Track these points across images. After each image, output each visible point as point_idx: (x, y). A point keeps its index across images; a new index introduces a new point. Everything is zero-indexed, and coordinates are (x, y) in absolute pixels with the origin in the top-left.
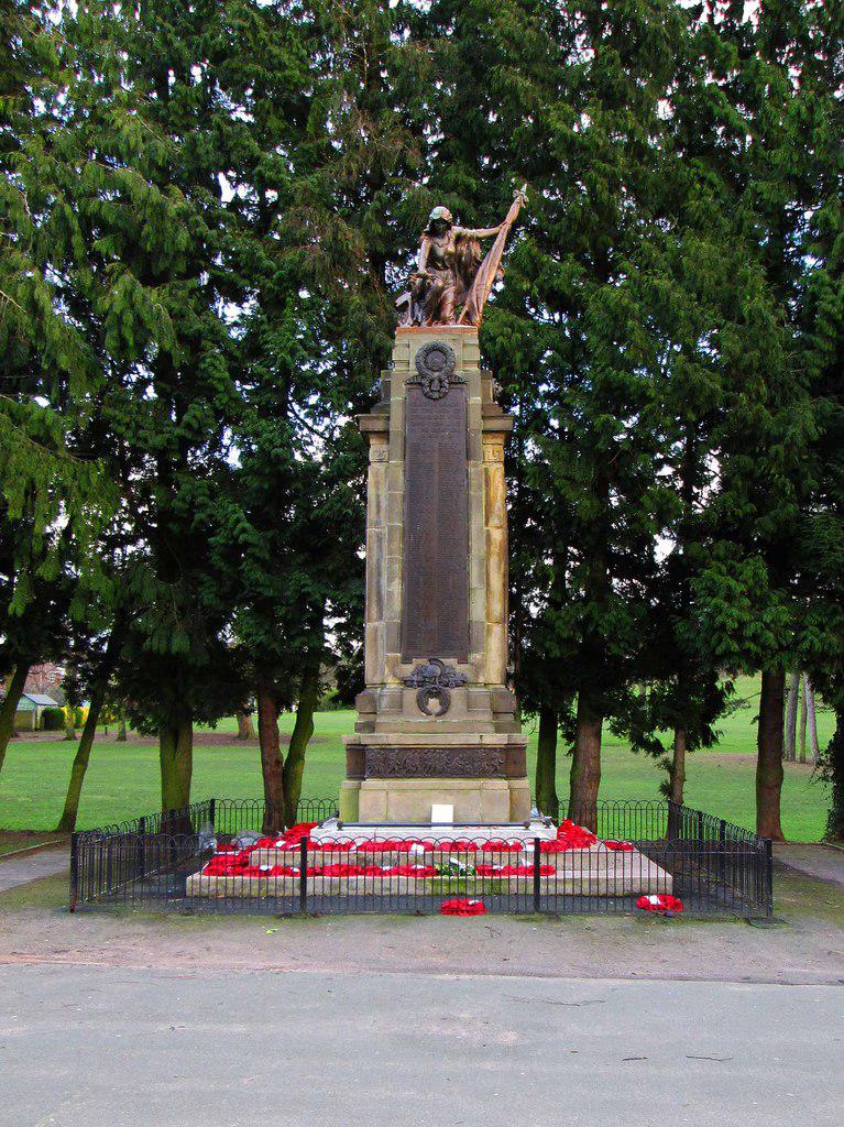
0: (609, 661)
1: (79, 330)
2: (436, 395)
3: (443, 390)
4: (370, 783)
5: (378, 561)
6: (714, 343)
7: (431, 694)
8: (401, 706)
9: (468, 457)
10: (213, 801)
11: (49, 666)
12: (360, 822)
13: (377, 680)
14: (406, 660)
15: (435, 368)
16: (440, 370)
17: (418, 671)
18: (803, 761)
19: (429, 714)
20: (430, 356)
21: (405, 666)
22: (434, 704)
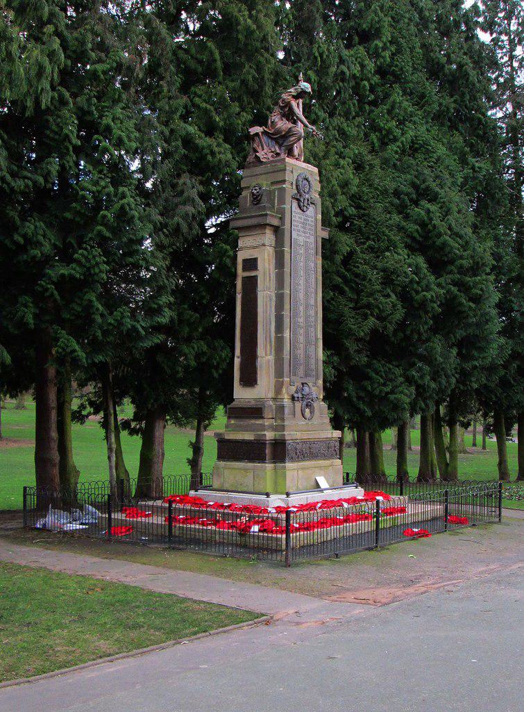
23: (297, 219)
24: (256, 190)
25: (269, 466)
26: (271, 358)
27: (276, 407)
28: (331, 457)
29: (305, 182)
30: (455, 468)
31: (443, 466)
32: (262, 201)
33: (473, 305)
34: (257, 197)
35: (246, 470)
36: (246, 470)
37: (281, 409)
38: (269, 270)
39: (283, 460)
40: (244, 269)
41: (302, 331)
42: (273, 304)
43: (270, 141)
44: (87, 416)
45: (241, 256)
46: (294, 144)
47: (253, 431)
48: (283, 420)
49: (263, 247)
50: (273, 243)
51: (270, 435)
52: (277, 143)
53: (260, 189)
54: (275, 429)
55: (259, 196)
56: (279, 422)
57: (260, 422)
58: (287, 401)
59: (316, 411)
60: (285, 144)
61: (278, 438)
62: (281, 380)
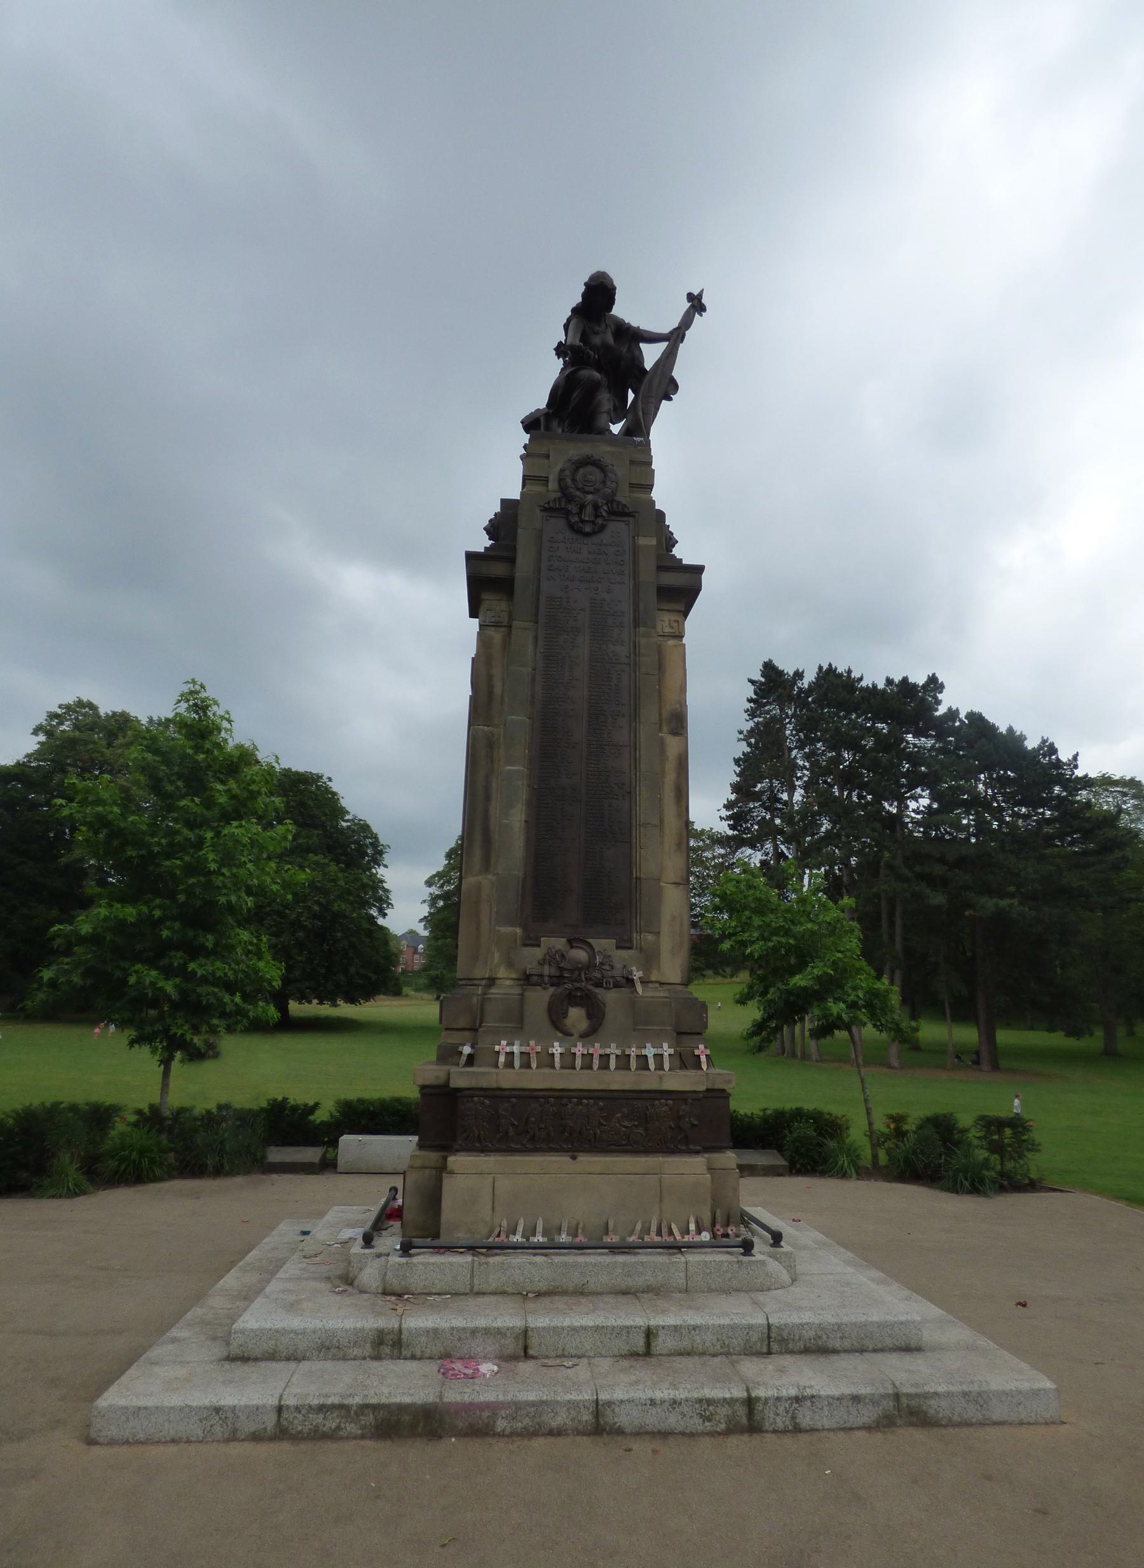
0: (860, 875)
2: (588, 528)
3: (600, 521)
4: (457, 1161)
6: (839, 869)
7: (572, 999)
9: (636, 623)
12: (443, 1240)
13: (480, 972)
14: (531, 941)
15: (587, 489)
16: (597, 491)
17: (551, 958)
20: (581, 471)
22: (576, 1016)
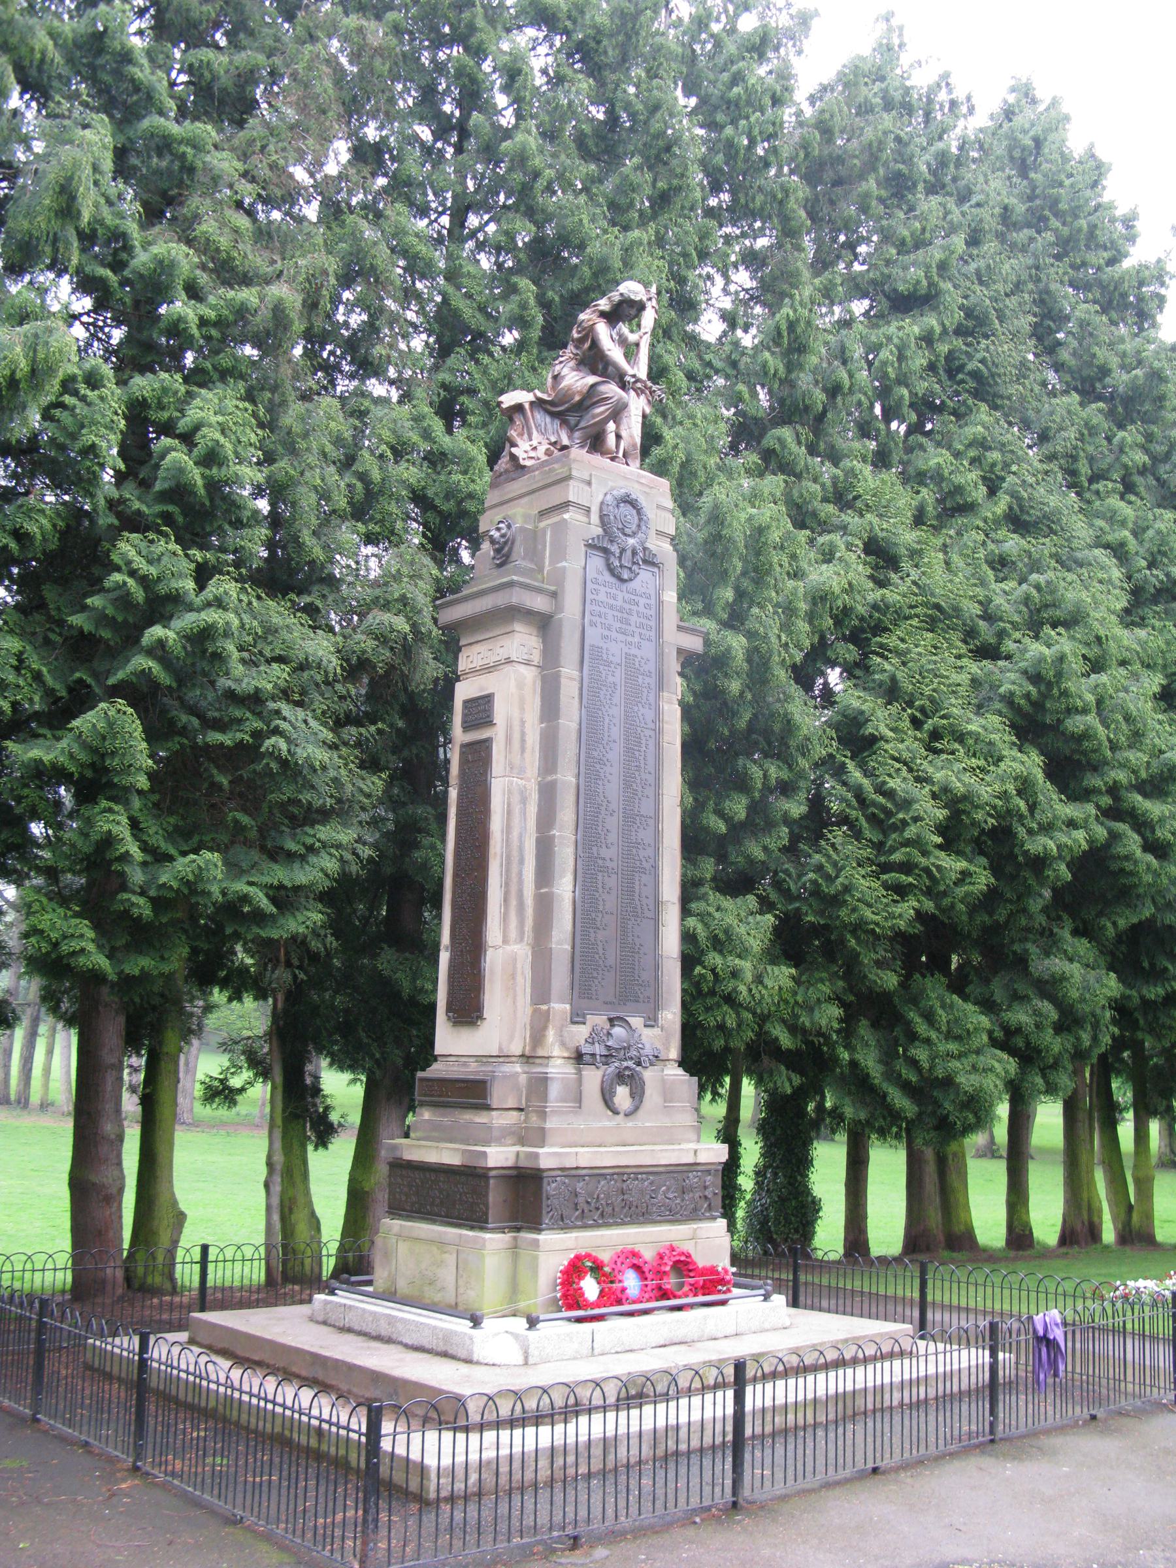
1: (338, 70)
5: (521, 837)
7: (621, 1077)
8: (580, 1101)
10: (205, 1249)
11: (1129, 1094)
18: (45, 1106)
19: (616, 1112)
21: (576, 1028)
23: (602, 597)
24: (498, 529)
25: (494, 1242)
26: (522, 951)
27: (530, 1080)
28: (694, 1215)
29: (626, 509)
30: (1149, 1216)
31: (1123, 1210)
32: (514, 556)
33: (1154, 862)
34: (502, 548)
35: (442, 1244)
36: (442, 1244)
37: (540, 1085)
38: (523, 722)
39: (535, 1225)
40: (467, 727)
41: (612, 882)
42: (533, 809)
43: (548, 419)
44: (242, 1090)
45: (463, 691)
46: (605, 421)
47: (463, 1142)
48: (543, 1114)
49: (508, 668)
50: (536, 658)
51: (499, 1156)
52: (564, 423)
53: (509, 527)
54: (523, 1137)
55: (506, 543)
56: (534, 1120)
57: (481, 1118)
58: (559, 1068)
59: (649, 1091)
60: (582, 424)
61: (523, 1163)
62: (544, 1007)
